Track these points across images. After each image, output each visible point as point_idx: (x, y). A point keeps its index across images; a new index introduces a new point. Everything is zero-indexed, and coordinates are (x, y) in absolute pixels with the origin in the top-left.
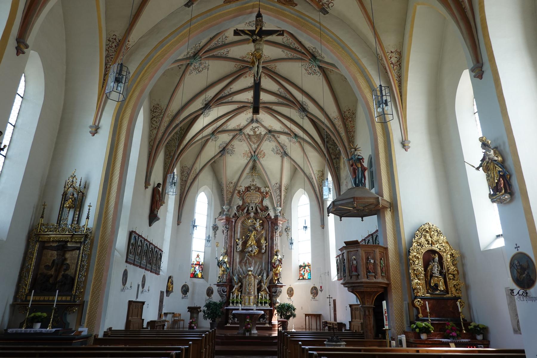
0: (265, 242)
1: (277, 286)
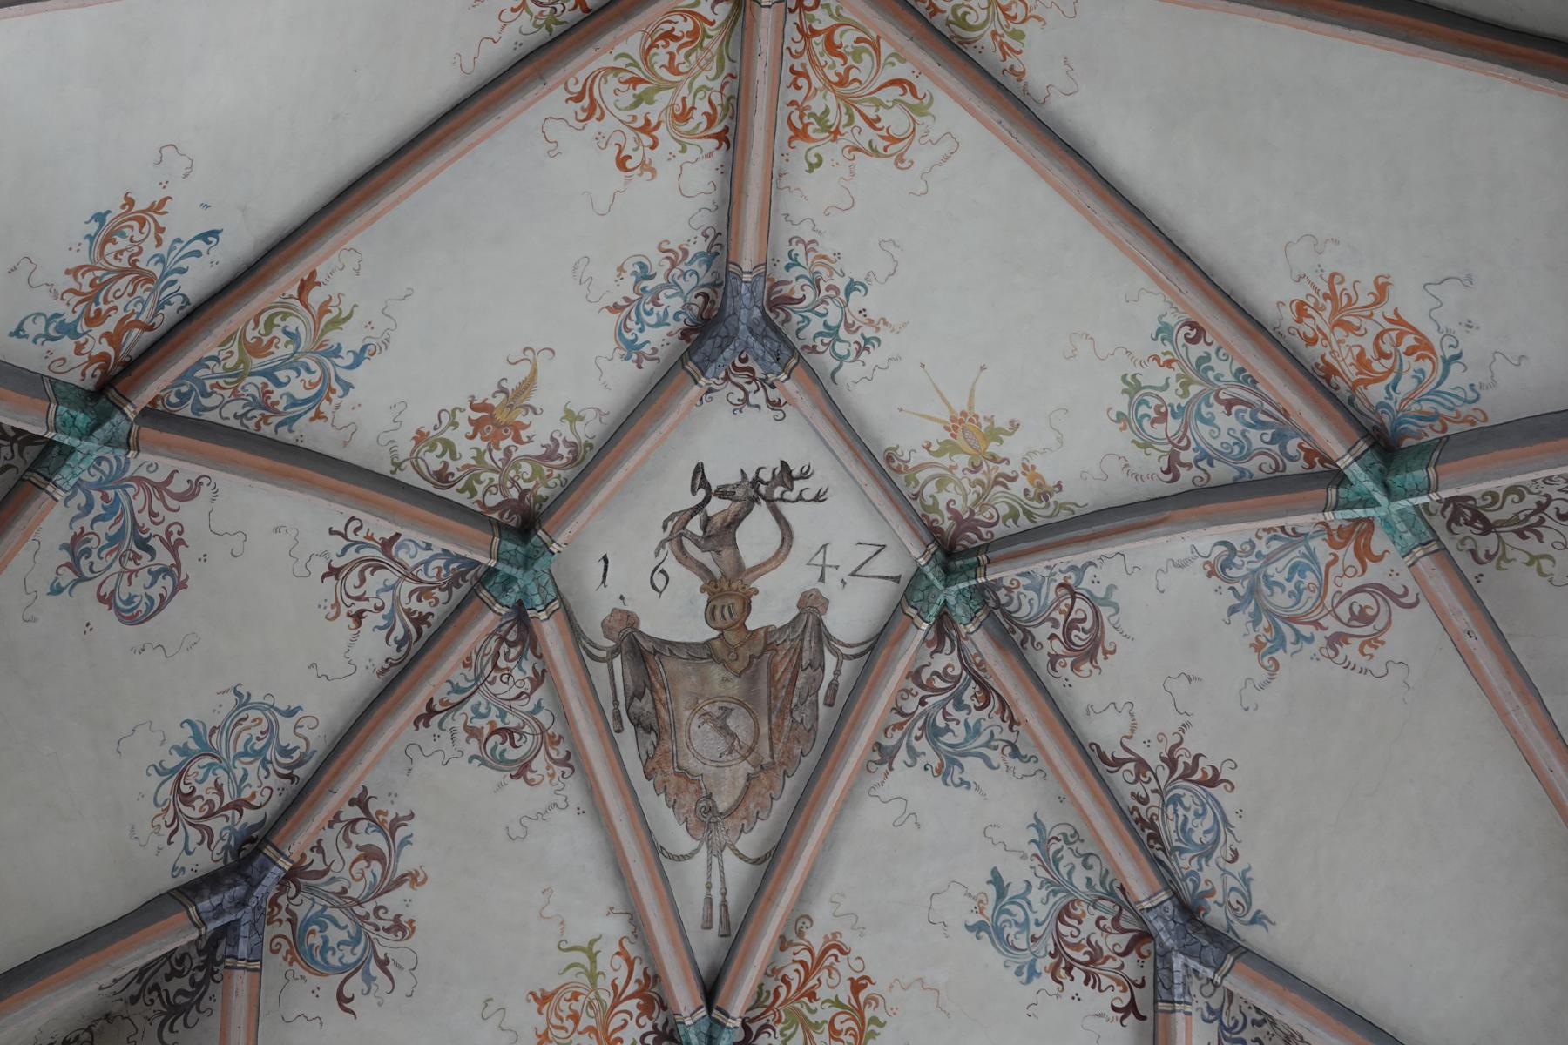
0: (1063, 568)
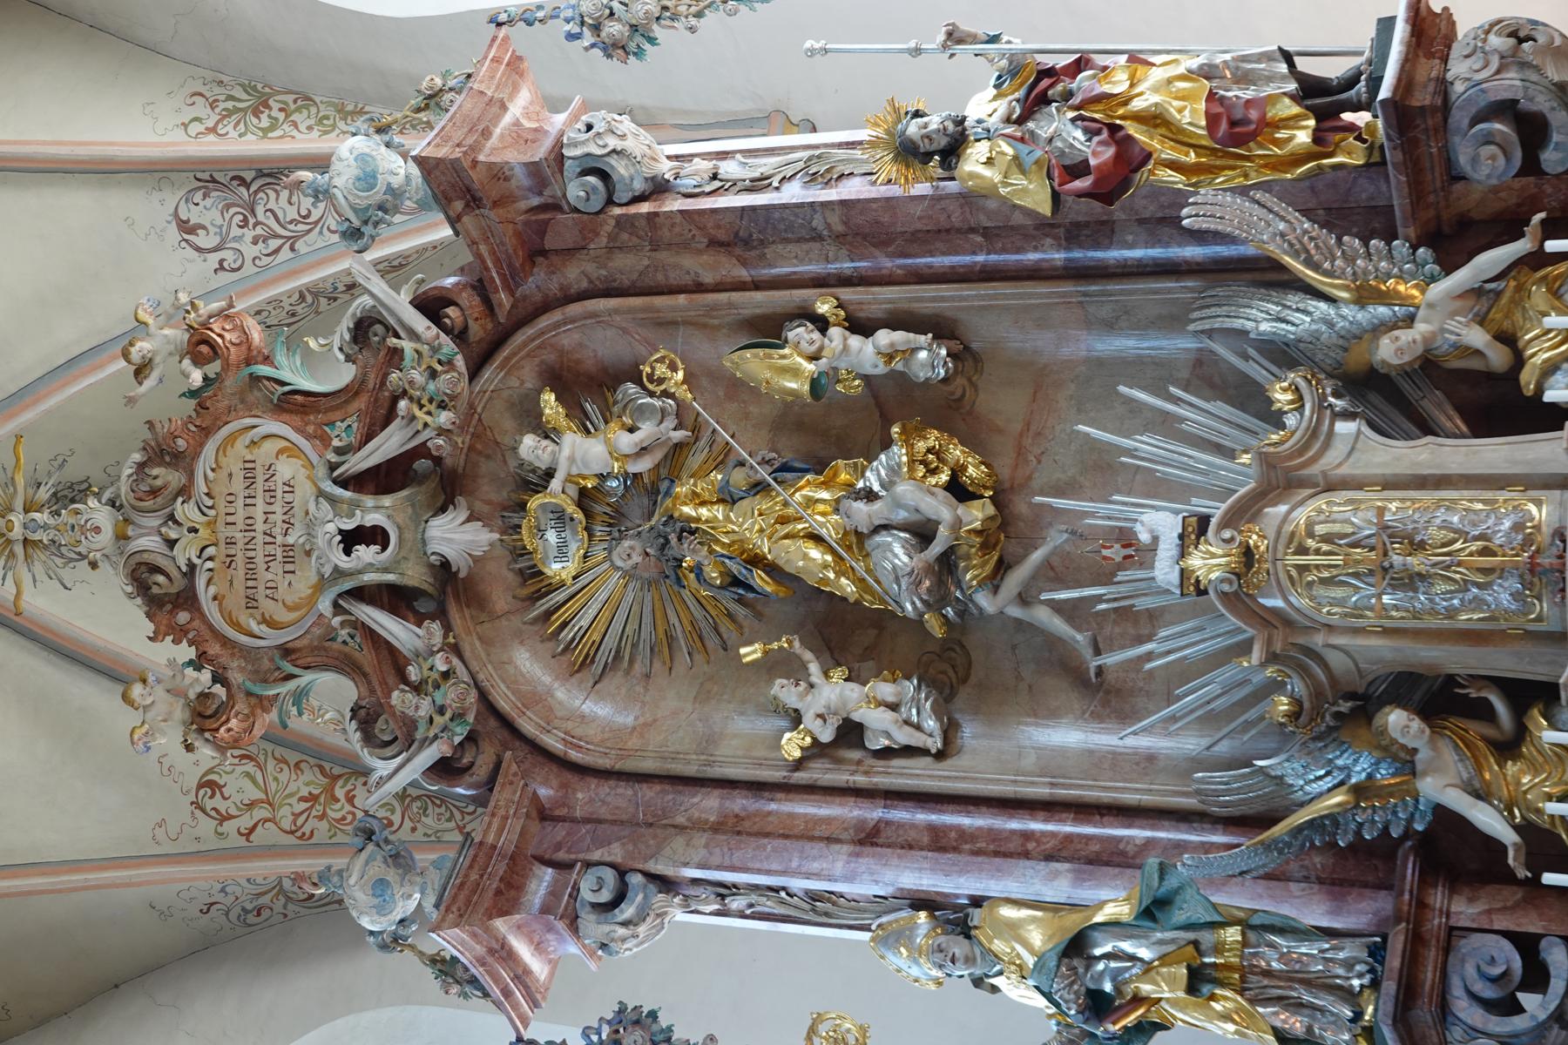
0: (801, 334)
1: (1423, 98)
